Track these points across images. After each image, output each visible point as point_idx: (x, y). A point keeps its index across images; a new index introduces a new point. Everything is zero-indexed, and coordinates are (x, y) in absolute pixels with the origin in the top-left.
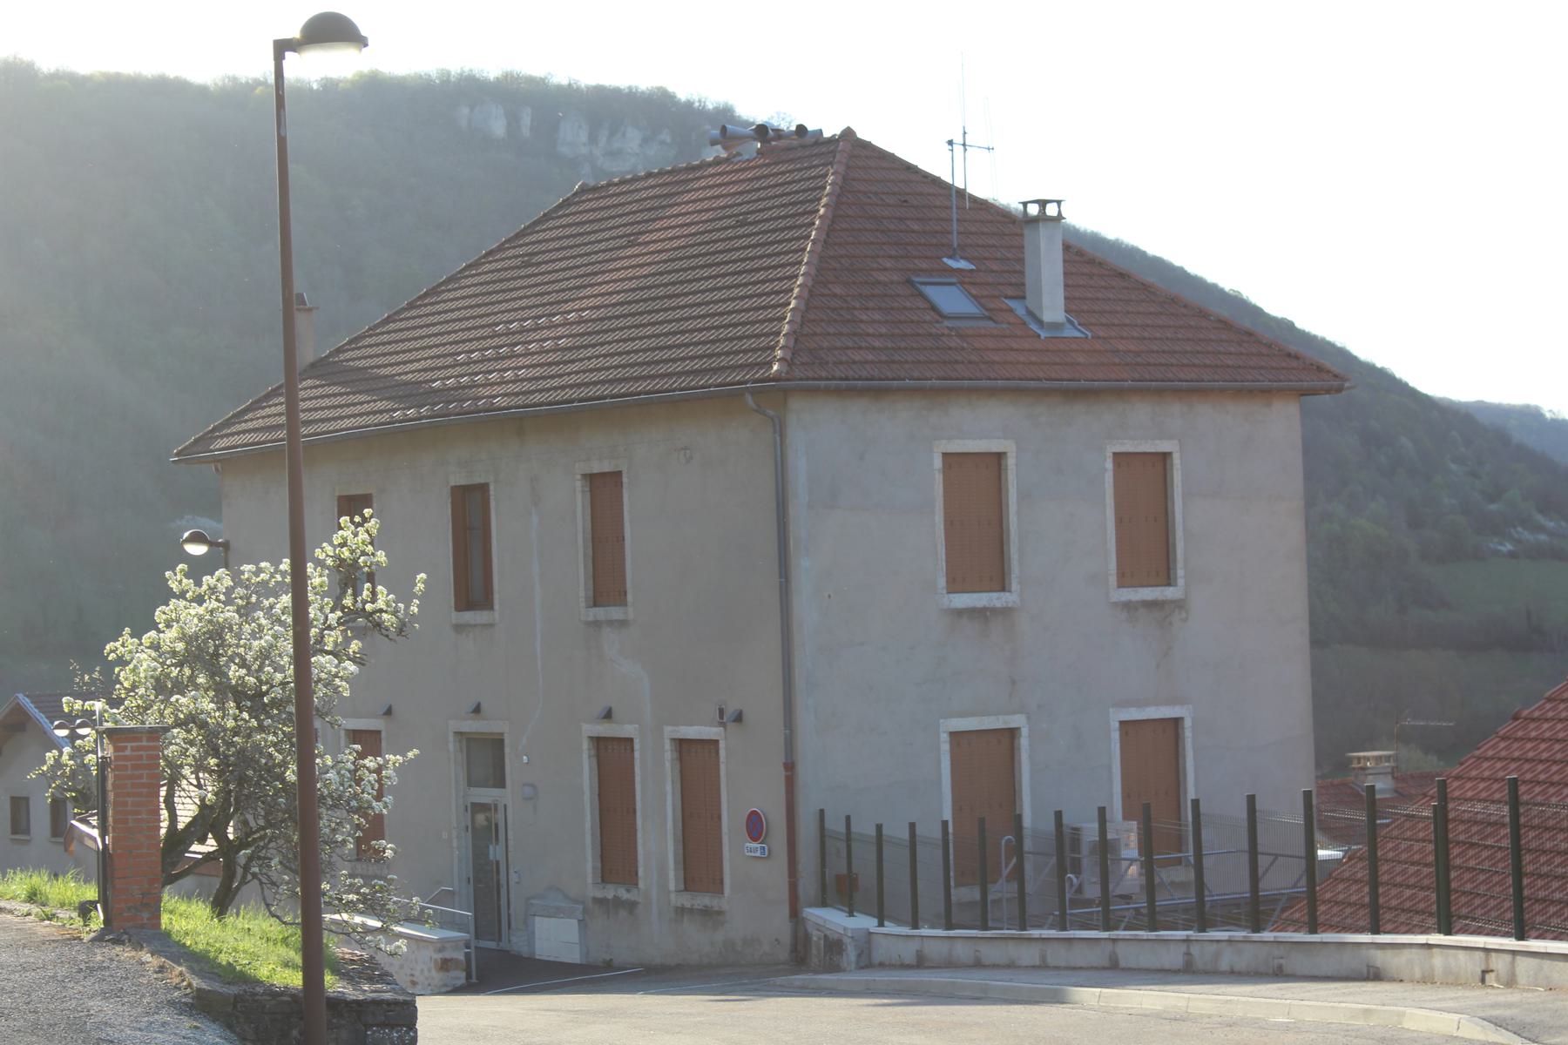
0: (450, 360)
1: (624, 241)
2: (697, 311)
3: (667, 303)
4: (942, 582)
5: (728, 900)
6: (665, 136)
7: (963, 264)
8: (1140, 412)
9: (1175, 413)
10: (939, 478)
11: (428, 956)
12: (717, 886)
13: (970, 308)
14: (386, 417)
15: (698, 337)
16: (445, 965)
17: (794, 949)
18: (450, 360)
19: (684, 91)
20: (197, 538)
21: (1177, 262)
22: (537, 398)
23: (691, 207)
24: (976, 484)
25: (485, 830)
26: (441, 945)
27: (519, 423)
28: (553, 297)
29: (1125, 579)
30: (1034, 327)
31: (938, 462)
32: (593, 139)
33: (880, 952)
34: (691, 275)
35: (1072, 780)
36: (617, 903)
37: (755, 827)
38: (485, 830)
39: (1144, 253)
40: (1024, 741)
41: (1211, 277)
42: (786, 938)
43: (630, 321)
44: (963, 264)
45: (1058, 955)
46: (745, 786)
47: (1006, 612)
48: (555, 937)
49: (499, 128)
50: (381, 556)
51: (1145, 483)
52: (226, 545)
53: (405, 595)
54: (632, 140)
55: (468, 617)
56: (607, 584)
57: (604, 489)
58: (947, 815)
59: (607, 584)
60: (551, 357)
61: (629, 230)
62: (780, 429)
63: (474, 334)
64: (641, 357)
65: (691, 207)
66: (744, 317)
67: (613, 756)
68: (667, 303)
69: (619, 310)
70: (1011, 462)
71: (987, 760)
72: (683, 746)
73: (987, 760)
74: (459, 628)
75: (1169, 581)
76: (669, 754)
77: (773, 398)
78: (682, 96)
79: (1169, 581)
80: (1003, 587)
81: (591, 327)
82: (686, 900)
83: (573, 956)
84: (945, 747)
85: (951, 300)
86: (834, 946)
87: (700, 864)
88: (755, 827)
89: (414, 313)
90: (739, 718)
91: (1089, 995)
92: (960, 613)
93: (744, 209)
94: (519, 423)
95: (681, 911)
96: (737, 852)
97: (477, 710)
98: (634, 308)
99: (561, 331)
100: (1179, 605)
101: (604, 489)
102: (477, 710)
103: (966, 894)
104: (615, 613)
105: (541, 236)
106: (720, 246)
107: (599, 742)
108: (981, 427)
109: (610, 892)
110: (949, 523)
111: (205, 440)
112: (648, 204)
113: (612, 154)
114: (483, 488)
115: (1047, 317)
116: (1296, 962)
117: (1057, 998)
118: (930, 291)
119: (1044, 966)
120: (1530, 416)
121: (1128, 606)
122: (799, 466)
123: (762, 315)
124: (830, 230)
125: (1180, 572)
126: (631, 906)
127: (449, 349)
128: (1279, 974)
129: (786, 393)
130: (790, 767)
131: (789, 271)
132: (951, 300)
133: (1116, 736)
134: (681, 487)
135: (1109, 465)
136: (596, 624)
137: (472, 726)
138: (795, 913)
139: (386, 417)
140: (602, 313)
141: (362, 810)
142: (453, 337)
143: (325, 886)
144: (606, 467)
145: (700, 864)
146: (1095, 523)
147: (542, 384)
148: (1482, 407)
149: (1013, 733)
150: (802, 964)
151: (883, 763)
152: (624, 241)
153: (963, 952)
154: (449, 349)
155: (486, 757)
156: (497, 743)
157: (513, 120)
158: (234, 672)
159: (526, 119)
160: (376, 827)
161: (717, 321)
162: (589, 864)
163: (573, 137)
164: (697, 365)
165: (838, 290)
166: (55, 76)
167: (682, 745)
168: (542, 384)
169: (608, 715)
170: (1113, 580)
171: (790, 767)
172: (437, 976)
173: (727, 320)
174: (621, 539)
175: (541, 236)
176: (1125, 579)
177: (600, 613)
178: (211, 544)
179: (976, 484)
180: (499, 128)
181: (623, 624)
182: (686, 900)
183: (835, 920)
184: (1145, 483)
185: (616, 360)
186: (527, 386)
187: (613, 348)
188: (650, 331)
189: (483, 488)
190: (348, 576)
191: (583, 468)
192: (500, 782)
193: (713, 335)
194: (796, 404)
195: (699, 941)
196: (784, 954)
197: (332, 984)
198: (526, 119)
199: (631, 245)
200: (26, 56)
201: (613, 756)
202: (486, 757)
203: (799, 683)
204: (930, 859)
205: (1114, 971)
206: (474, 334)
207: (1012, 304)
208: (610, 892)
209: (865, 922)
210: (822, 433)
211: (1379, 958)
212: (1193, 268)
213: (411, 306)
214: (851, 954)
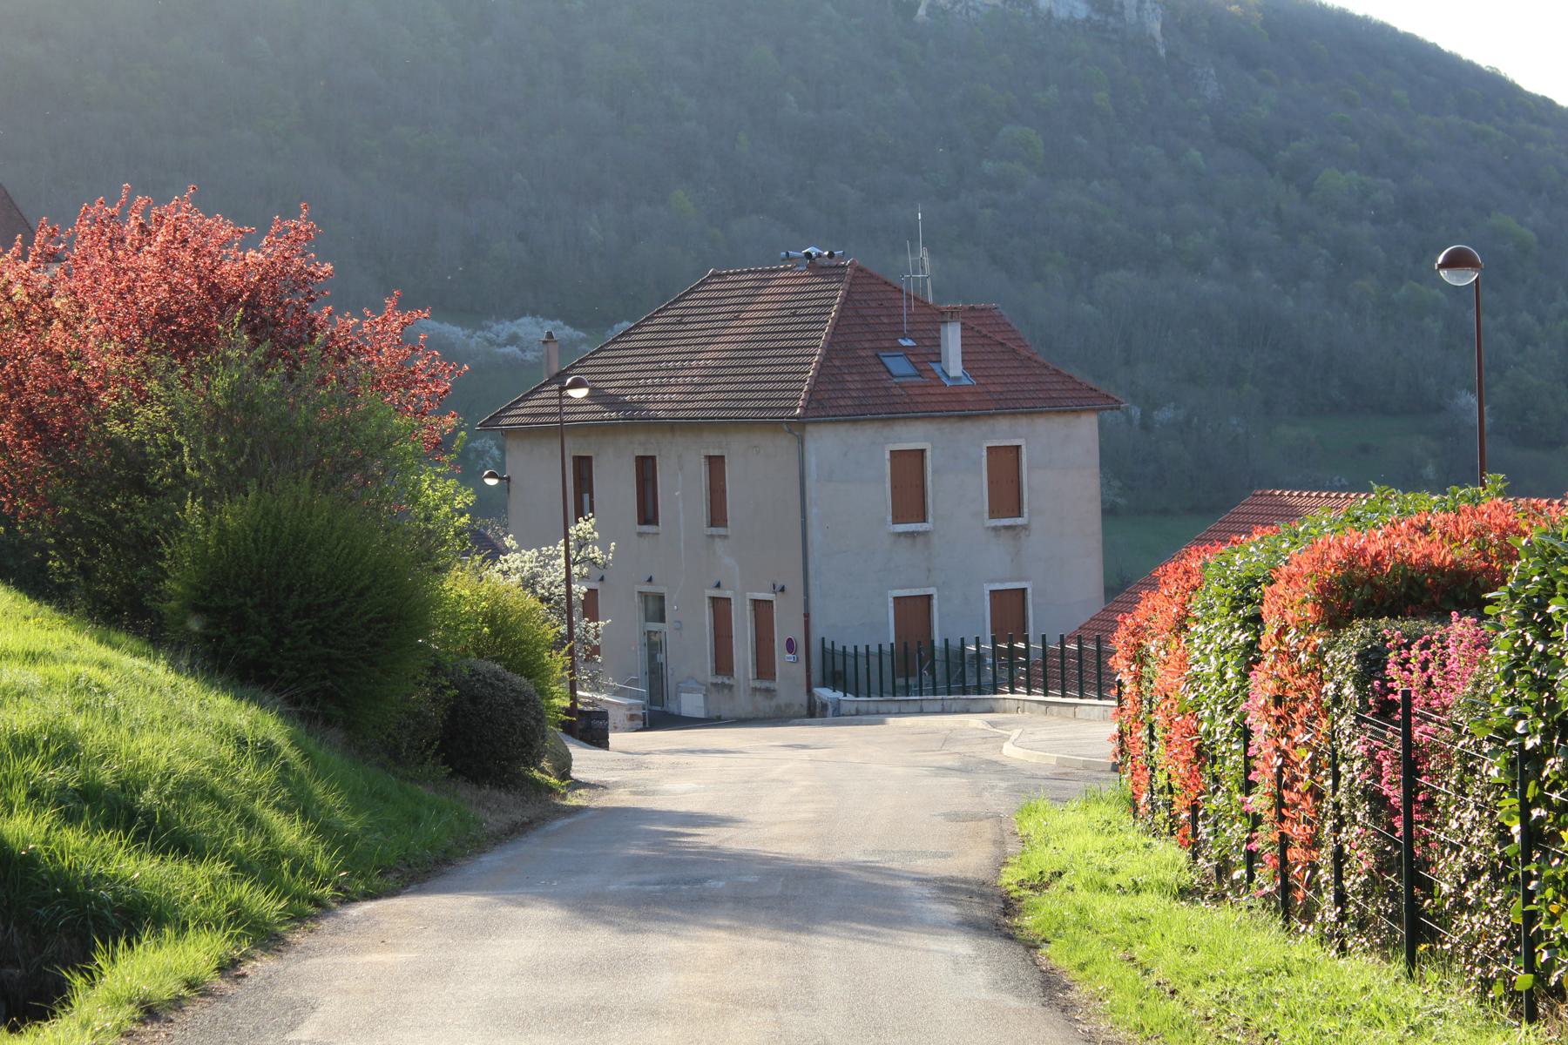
0: (635, 383)
1: (731, 316)
2: (765, 370)
3: (752, 362)
4: (890, 518)
5: (778, 684)
7: (909, 343)
8: (1003, 424)
9: (1023, 423)
10: (888, 465)
11: (625, 712)
12: (772, 676)
13: (910, 370)
14: (599, 416)
15: (764, 386)
16: (632, 717)
17: (809, 708)
18: (635, 383)
20: (492, 475)
21: (1430, 39)
22: (681, 414)
23: (769, 298)
24: (909, 467)
25: (654, 647)
26: (630, 707)
27: (673, 426)
28: (693, 348)
29: (994, 513)
30: (944, 379)
31: (888, 456)
33: (845, 708)
34: (765, 345)
35: (962, 622)
36: (724, 685)
38: (654, 647)
39: (1394, 30)
40: (935, 602)
41: (1466, 54)
42: (805, 703)
43: (731, 371)
44: (909, 343)
45: (883, 707)
46: (786, 626)
47: (925, 533)
48: (691, 704)
50: (596, 535)
51: (1005, 464)
52: (508, 479)
53: (606, 551)
55: (645, 528)
56: (717, 516)
57: (716, 464)
58: (892, 640)
59: (717, 516)
60: (690, 388)
61: (736, 308)
62: (802, 442)
63: (649, 366)
64: (734, 395)
65: (769, 298)
66: (786, 377)
67: (720, 607)
68: (752, 362)
69: (726, 363)
70: (928, 454)
72: (756, 603)
73: (915, 611)
74: (640, 534)
75: (1020, 515)
76: (749, 607)
77: (797, 427)
79: (1020, 515)
80: (924, 520)
81: (710, 372)
82: (758, 684)
83: (701, 714)
84: (891, 605)
85: (899, 365)
86: (824, 706)
87: (764, 667)
89: (615, 346)
90: (782, 590)
91: (891, 720)
92: (899, 534)
93: (796, 304)
94: (673, 426)
95: (755, 690)
96: (781, 657)
97: (650, 580)
98: (734, 363)
99: (695, 372)
100: (1025, 527)
101: (716, 464)
102: (650, 580)
103: (901, 681)
104: (721, 531)
105: (689, 304)
106: (781, 328)
107: (714, 600)
108: (910, 436)
109: (719, 680)
110: (894, 487)
111: (495, 418)
112: (747, 292)
114: (653, 458)
115: (952, 374)
116: (973, 706)
117: (882, 723)
118: (886, 360)
119: (878, 713)
121: (995, 529)
122: (812, 460)
123: (788, 394)
124: (836, 326)
125: (1026, 510)
126: (730, 687)
127: (635, 375)
128: (968, 712)
129: (804, 424)
130: (807, 615)
131: (803, 368)
132: (899, 365)
133: (988, 598)
134: (755, 466)
135: (985, 453)
136: (712, 536)
137: (647, 588)
138: (809, 691)
139: (599, 416)
140: (717, 363)
141: (589, 644)
142: (637, 367)
144: (716, 453)
145: (764, 667)
147: (684, 406)
149: (929, 597)
150: (813, 712)
152: (731, 316)
153: (872, 707)
154: (635, 375)
155: (655, 607)
156: (661, 598)
158: (540, 591)
160: (596, 650)
161: (774, 378)
162: (709, 664)
164: (762, 404)
165: (837, 363)
167: (756, 602)
168: (684, 406)
169: (718, 586)
170: (986, 515)
171: (807, 615)
172: (628, 724)
173: (779, 377)
174: (724, 491)
175: (689, 304)
176: (994, 513)
177: (714, 531)
178: (501, 479)
179: (909, 467)
181: (726, 537)
182: (758, 684)
183: (825, 694)
184: (1005, 464)
185: (722, 396)
186: (675, 406)
187: (722, 387)
188: (740, 379)
189: (653, 458)
190: (582, 543)
191: (705, 452)
192: (662, 619)
193: (770, 386)
194: (810, 428)
195: (764, 705)
196: (805, 712)
197: (580, 706)
199: (737, 318)
201: (720, 607)
202: (655, 607)
203: (811, 572)
204: (887, 660)
205: (900, 713)
206: (649, 366)
207: (934, 366)
208: (719, 680)
209: (839, 695)
210: (825, 443)
211: (993, 703)
212: (1447, 45)
213: (614, 341)
214: (830, 710)
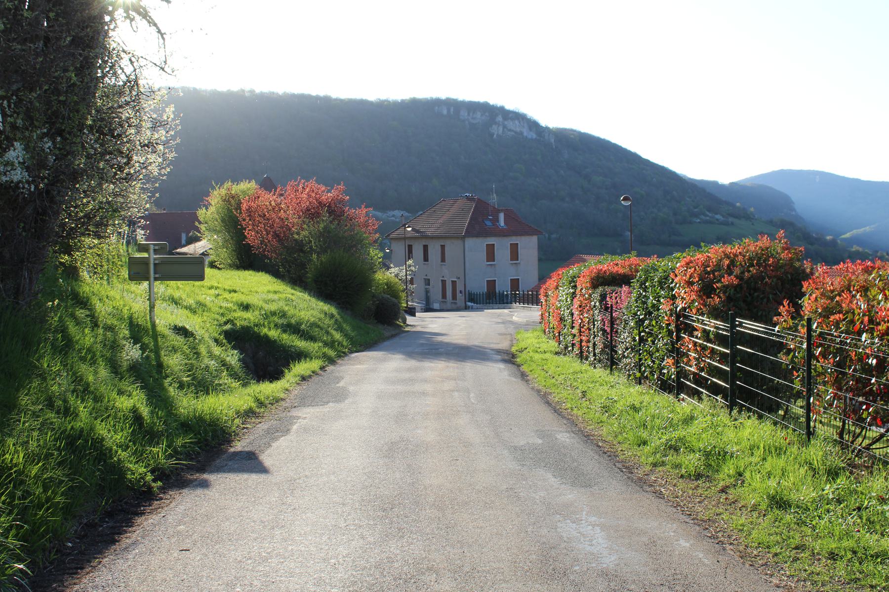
6: (487, 114)
8: (514, 238)
19: (492, 102)
24: (491, 249)
25: (427, 292)
27: (432, 238)
32: (469, 114)
37: (461, 292)
38: (427, 292)
46: (460, 287)
49: (445, 112)
51: (514, 248)
54: (478, 115)
56: (443, 260)
57: (443, 247)
59: (443, 260)
67: (444, 282)
71: (491, 284)
72: (453, 281)
73: (491, 284)
77: (463, 238)
78: (491, 103)
87: (454, 297)
88: (461, 292)
94: (432, 238)
96: (459, 295)
101: (443, 247)
108: (491, 241)
113: (473, 118)
120: (715, 184)
122: (466, 246)
134: (452, 248)
143: (828, 238)
145: (454, 297)
146: (508, 252)
148: (702, 181)
150: (466, 308)
151: (479, 286)
155: (427, 282)
157: (449, 110)
159: (452, 110)
163: (464, 114)
166: (336, 100)
179: (491, 249)
180: (445, 112)
183: (469, 304)
184: (514, 248)
190: (410, 266)
195: (454, 306)
198: (452, 110)
200: (329, 94)
201: (444, 282)
202: (427, 282)
210: (470, 242)
212: (624, 146)
